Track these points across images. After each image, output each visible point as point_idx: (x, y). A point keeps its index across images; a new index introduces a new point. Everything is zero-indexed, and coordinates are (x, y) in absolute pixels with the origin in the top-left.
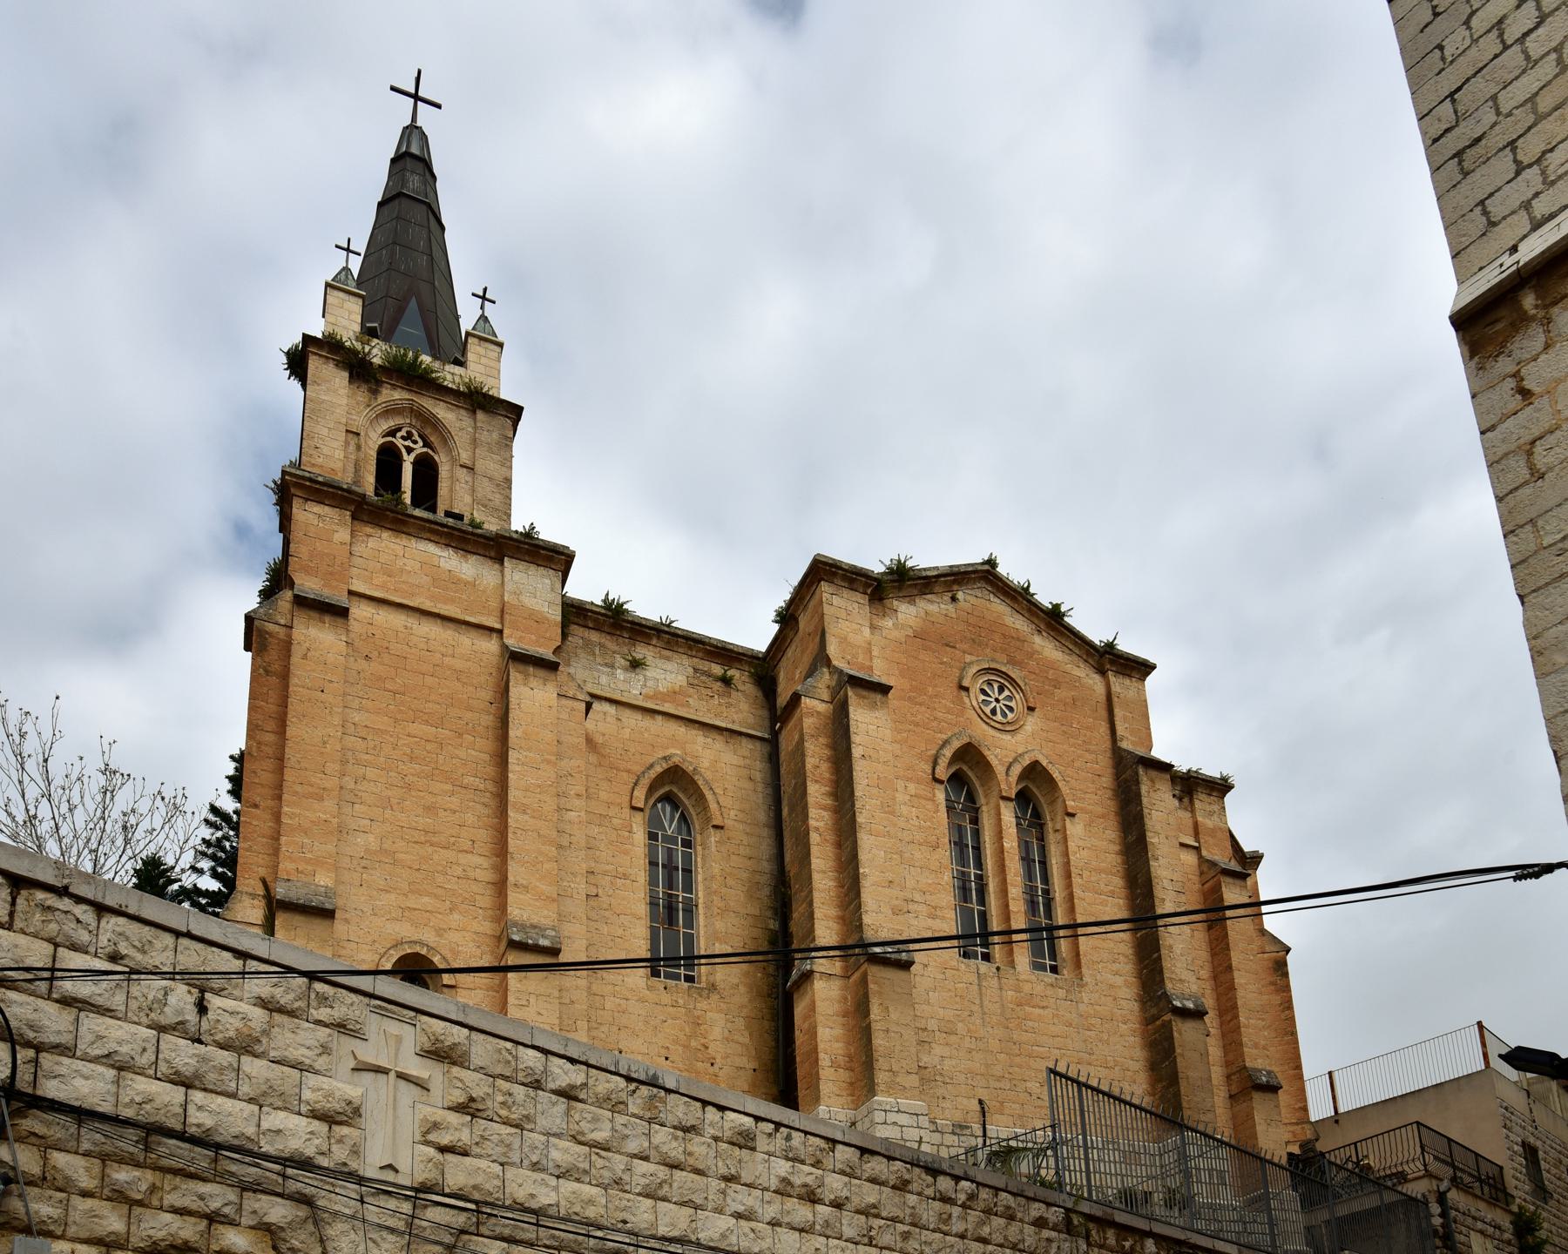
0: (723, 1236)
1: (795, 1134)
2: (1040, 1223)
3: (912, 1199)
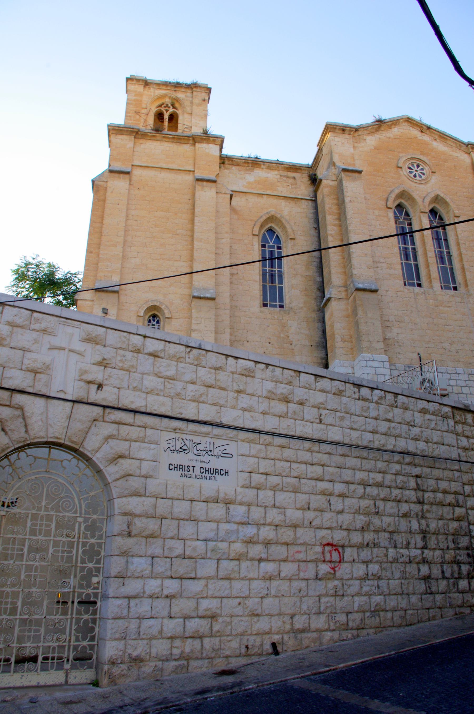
0: (235, 419)
2: (424, 411)
3: (345, 400)
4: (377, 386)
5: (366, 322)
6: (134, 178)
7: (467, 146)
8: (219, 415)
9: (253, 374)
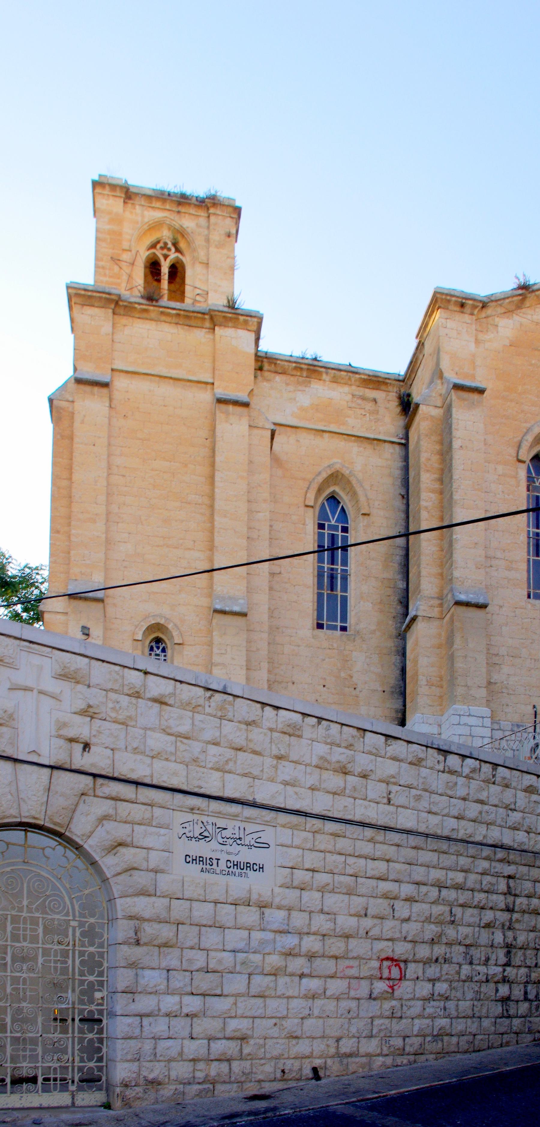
3: (424, 772)
4: (471, 753)
5: (466, 657)
8: (251, 789)
9: (300, 733)
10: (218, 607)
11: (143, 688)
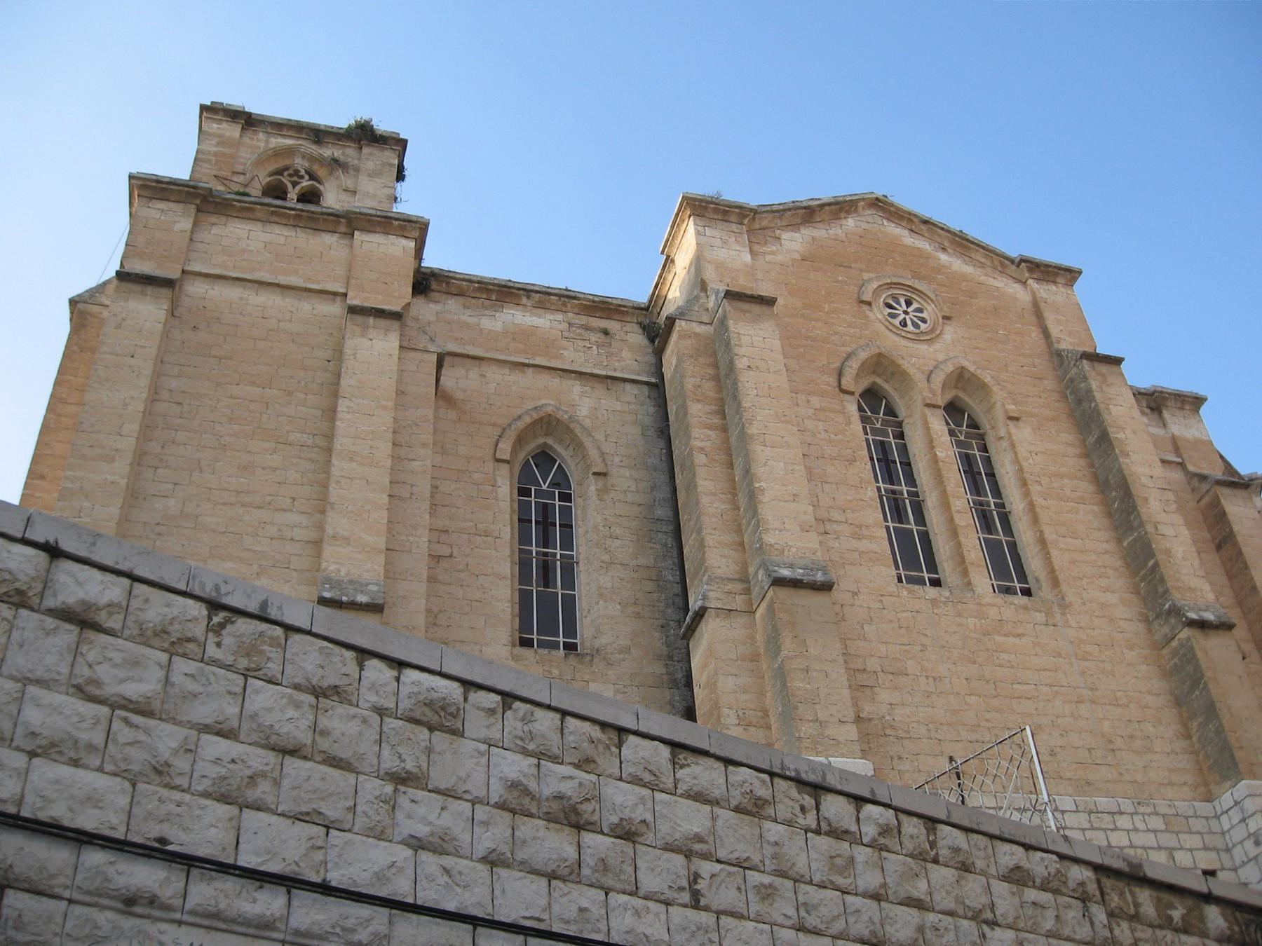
0: (380, 877)
1: (539, 713)
2: (1018, 877)
3: (774, 831)
6: (185, 302)
7: (1018, 266)
8: (319, 856)
10: (327, 595)
11: (39, 587)
